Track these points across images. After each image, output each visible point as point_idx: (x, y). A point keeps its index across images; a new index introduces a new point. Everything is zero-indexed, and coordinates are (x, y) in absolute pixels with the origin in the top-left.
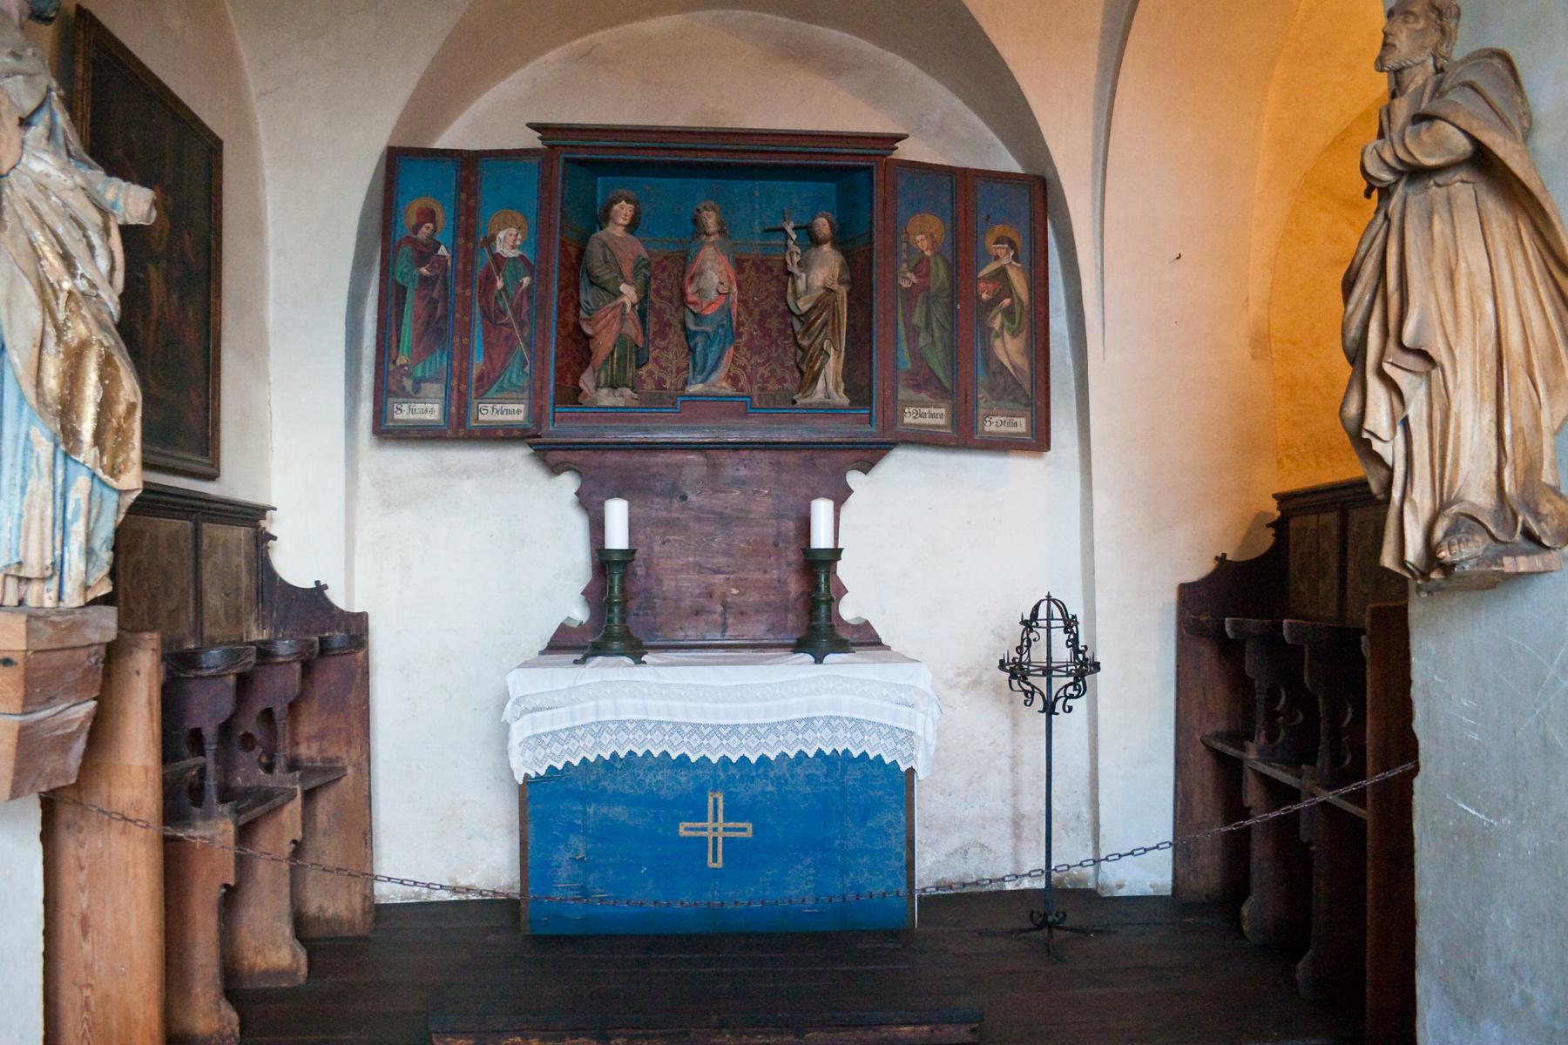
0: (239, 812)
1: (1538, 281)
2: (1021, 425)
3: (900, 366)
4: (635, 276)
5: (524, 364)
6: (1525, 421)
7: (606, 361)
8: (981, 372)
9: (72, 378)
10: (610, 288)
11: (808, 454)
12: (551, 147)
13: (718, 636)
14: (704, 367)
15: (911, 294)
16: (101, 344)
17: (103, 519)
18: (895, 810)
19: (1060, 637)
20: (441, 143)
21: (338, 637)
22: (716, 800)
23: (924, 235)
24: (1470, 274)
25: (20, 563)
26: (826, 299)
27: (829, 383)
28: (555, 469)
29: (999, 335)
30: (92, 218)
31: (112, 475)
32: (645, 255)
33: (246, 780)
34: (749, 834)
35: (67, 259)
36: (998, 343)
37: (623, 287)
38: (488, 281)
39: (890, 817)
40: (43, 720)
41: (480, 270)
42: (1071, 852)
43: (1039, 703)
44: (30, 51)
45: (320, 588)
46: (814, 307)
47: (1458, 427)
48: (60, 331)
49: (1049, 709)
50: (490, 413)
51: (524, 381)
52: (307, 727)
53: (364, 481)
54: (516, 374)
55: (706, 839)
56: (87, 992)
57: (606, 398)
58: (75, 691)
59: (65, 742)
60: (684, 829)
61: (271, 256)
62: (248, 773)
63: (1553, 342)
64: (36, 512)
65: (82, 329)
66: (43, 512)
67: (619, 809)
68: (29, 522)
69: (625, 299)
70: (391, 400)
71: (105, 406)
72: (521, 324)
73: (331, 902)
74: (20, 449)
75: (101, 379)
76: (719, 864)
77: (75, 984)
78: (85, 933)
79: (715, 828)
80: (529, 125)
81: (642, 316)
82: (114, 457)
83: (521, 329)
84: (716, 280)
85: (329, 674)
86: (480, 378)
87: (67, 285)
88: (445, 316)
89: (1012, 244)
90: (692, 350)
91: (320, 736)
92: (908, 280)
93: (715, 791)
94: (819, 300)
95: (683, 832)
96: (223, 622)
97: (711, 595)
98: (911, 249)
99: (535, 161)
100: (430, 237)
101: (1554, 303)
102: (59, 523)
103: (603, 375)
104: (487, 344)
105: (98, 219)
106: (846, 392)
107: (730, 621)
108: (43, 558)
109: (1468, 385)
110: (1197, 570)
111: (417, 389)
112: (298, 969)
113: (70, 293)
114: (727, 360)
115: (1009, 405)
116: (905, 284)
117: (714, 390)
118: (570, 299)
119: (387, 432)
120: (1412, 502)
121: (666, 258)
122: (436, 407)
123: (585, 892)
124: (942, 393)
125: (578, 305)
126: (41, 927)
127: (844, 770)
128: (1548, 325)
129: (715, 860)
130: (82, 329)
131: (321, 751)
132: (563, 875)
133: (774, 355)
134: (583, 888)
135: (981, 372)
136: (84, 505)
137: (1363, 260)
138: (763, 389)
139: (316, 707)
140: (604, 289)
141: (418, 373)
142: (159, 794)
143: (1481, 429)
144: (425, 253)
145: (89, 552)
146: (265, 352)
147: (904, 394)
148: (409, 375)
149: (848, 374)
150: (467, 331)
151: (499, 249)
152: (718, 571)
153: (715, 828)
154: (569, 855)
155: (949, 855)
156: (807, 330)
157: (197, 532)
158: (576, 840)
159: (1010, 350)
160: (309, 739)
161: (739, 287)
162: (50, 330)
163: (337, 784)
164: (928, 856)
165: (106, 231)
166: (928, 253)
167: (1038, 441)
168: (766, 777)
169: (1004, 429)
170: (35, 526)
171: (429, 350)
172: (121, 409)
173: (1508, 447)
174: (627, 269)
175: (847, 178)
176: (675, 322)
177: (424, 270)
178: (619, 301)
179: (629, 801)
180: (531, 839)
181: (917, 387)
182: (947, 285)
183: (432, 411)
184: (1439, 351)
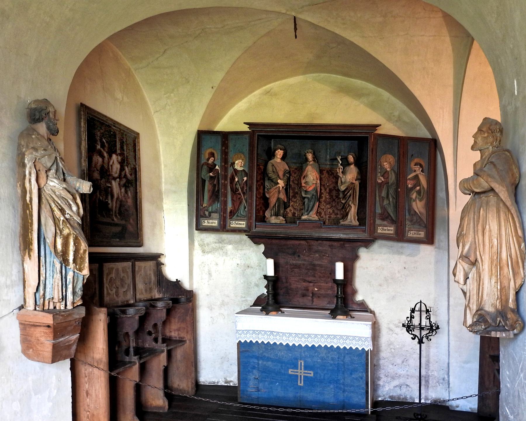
2: (422, 234)
3: (377, 211)
4: (284, 175)
5: (245, 208)
7: (274, 207)
8: (407, 214)
9: (66, 245)
10: (274, 180)
11: (342, 243)
12: (253, 131)
13: (310, 304)
14: (308, 210)
15: (381, 185)
16: (74, 234)
17: (78, 283)
18: (362, 372)
19: (424, 315)
20: (216, 129)
21: (183, 299)
23: (387, 163)
24: (490, 231)
27: (352, 218)
28: (257, 243)
30: (69, 197)
32: (288, 168)
33: (149, 345)
34: (312, 375)
35: (62, 211)
36: (414, 204)
37: (279, 181)
38: (233, 179)
39: (360, 375)
40: (61, 341)
42: (433, 394)
43: (417, 340)
44: (50, 147)
47: (483, 284)
49: (421, 342)
50: (234, 224)
53: (196, 243)
55: (297, 376)
56: (88, 413)
57: (274, 220)
58: (73, 333)
59: (69, 347)
60: (290, 372)
61: (163, 166)
62: (149, 343)
64: (56, 284)
66: (58, 284)
67: (270, 363)
69: (280, 185)
70: (201, 219)
71: (76, 252)
72: (244, 193)
73: (181, 384)
74: (52, 265)
75: (74, 244)
76: (302, 384)
77: (85, 410)
78: (87, 396)
80: (244, 123)
81: (286, 190)
82: (80, 265)
83: (244, 196)
84: (312, 178)
85: (180, 310)
86: (231, 212)
88: (218, 190)
89: (421, 166)
90: (304, 203)
91: (178, 330)
92: (380, 179)
93: (301, 360)
95: (290, 372)
96: (144, 293)
97: (308, 290)
98: (382, 167)
99: (247, 136)
100: (213, 162)
102: (64, 286)
103: (273, 212)
104: (232, 200)
105: (71, 197)
106: (358, 220)
108: (59, 297)
111: (210, 216)
112: (165, 406)
115: (418, 227)
116: (380, 181)
117: (311, 218)
119: (200, 228)
123: (258, 390)
124: (393, 222)
125: (264, 188)
126: (71, 394)
127: (344, 357)
129: (301, 383)
131: (178, 334)
132: (252, 383)
133: (334, 205)
135: (407, 214)
136: (72, 280)
138: (330, 217)
139: (177, 320)
140: (273, 181)
144: (212, 168)
145: (74, 293)
147: (378, 222)
148: (207, 210)
150: (226, 196)
151: (236, 167)
152: (310, 282)
153: (301, 372)
155: (395, 387)
157: (133, 266)
158: (255, 371)
159: (419, 206)
160: (175, 330)
162: (58, 231)
163: (183, 346)
165: (74, 199)
166: (388, 170)
167: (430, 240)
168: (318, 357)
169: (415, 236)
170: (56, 288)
171: (214, 202)
172: (82, 251)
174: (281, 174)
175: (359, 141)
176: (299, 192)
177: (211, 174)
178: (278, 186)
179: (272, 361)
180: (241, 370)
181: (383, 219)
182: (395, 182)
183: (215, 223)
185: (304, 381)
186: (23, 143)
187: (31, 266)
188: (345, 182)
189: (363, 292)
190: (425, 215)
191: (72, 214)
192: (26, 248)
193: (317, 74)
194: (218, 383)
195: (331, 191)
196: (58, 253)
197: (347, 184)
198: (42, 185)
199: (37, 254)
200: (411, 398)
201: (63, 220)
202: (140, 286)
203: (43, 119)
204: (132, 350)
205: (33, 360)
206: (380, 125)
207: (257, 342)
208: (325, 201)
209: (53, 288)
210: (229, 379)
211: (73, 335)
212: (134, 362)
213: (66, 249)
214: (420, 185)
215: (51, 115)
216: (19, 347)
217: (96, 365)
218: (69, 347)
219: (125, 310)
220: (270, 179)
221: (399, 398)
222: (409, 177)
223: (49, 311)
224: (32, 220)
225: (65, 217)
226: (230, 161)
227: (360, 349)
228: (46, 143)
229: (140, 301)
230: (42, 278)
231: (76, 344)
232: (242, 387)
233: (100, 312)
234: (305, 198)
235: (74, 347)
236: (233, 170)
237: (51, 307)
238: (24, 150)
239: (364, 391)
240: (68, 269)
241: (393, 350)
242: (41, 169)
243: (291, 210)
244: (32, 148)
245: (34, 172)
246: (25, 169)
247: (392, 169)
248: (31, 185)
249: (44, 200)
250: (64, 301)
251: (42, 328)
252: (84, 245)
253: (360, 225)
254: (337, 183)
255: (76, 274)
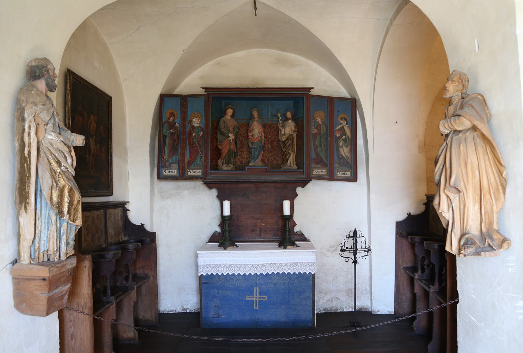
0: (117, 298)
1: (493, 165)
2: (348, 174)
3: (312, 157)
4: (234, 129)
5: (201, 158)
6: (489, 209)
8: (336, 158)
9: (61, 197)
10: (226, 134)
14: (254, 158)
21: (148, 240)
22: (256, 290)
24: (472, 163)
25: (47, 250)
26: (290, 137)
28: (210, 188)
29: (342, 147)
30: (65, 149)
31: (73, 222)
32: (237, 124)
35: (59, 163)
36: (341, 150)
37: (230, 135)
38: (190, 134)
39: (308, 295)
41: (188, 131)
42: (363, 303)
44: (48, 102)
45: (142, 225)
46: (286, 139)
47: (468, 211)
48: (57, 184)
51: (201, 163)
52: (139, 265)
53: (156, 191)
54: (199, 161)
55: (253, 301)
57: (225, 168)
58: (65, 283)
60: (247, 298)
61: (128, 126)
62: (121, 282)
63: (497, 185)
64: (52, 236)
65: (64, 183)
68: (50, 239)
70: (162, 169)
71: (71, 203)
72: (200, 146)
73: (146, 315)
74: (47, 218)
75: (69, 195)
78: (72, 340)
79: (256, 297)
80: (202, 88)
82: (74, 216)
84: (257, 132)
86: (188, 162)
87: (58, 171)
88: (178, 144)
89: (346, 120)
90: (251, 153)
92: (314, 131)
93: (256, 287)
94: (288, 137)
97: (256, 226)
99: (203, 98)
100: (173, 121)
101: (497, 173)
102: (59, 237)
105: (67, 150)
107: (262, 233)
108: (54, 249)
109: (471, 198)
110: (402, 217)
111: (170, 166)
113: (59, 173)
114: (261, 156)
116: (314, 133)
118: (214, 138)
119: (161, 177)
120: (454, 232)
121: (243, 125)
122: (176, 171)
123: (218, 316)
124: (324, 165)
125: (217, 140)
127: (294, 281)
128: (496, 180)
129: (256, 307)
130: (64, 183)
133: (275, 153)
134: (218, 314)
135: (336, 158)
136: (65, 231)
137: (440, 155)
140: (224, 135)
141: (170, 161)
142: (92, 301)
143: (475, 211)
144: (172, 125)
145: (67, 244)
146: (126, 154)
147: (313, 165)
148: (168, 161)
149: (296, 159)
150: (184, 148)
152: (258, 219)
153: (256, 297)
154: (214, 305)
156: (284, 146)
157: (105, 213)
159: (345, 151)
161: (264, 133)
162: (54, 184)
164: (321, 301)
167: (354, 178)
168: (271, 283)
169: (343, 175)
172: (75, 202)
173: (483, 217)
175: (297, 99)
176: (246, 144)
177: (171, 130)
180: (203, 300)
181: (317, 164)
184: (462, 187)
185: (259, 304)
186: (22, 98)
187: (26, 220)
188: (284, 134)
189: (301, 225)
190: (350, 158)
191: (67, 166)
192: (23, 202)
193: (259, 49)
194: (176, 310)
195: (272, 141)
196: (53, 205)
197: (287, 136)
198: (40, 139)
199: (34, 207)
200: (341, 308)
201: (59, 173)
202: (111, 231)
203: (43, 76)
204: (109, 290)
205: (26, 314)
206: (314, 88)
207: (217, 274)
208: (267, 150)
209: (48, 241)
210: (185, 307)
211: (66, 285)
212: (111, 302)
213: (61, 201)
214: (345, 135)
215: (51, 72)
216: (12, 302)
217: (80, 309)
218: (62, 297)
219: (104, 254)
220: (221, 133)
221: (331, 310)
222: (337, 128)
223: (42, 264)
224: (30, 173)
225: (61, 170)
226: (189, 119)
227: (308, 273)
228: (45, 98)
229: (111, 244)
230: (37, 231)
231: (68, 294)
232: (204, 315)
233: (85, 259)
234: (252, 148)
235: (66, 297)
236: (190, 126)
237: (46, 259)
238: (24, 104)
239: (311, 308)
240: (62, 220)
241: (326, 271)
242: (40, 123)
243: (239, 159)
244: (32, 103)
245: (33, 125)
246: (25, 123)
247: (323, 123)
248: (30, 139)
249: (42, 153)
250: (58, 253)
251: (37, 281)
252: (77, 196)
253: (298, 168)
254: (278, 135)
255: (69, 225)
